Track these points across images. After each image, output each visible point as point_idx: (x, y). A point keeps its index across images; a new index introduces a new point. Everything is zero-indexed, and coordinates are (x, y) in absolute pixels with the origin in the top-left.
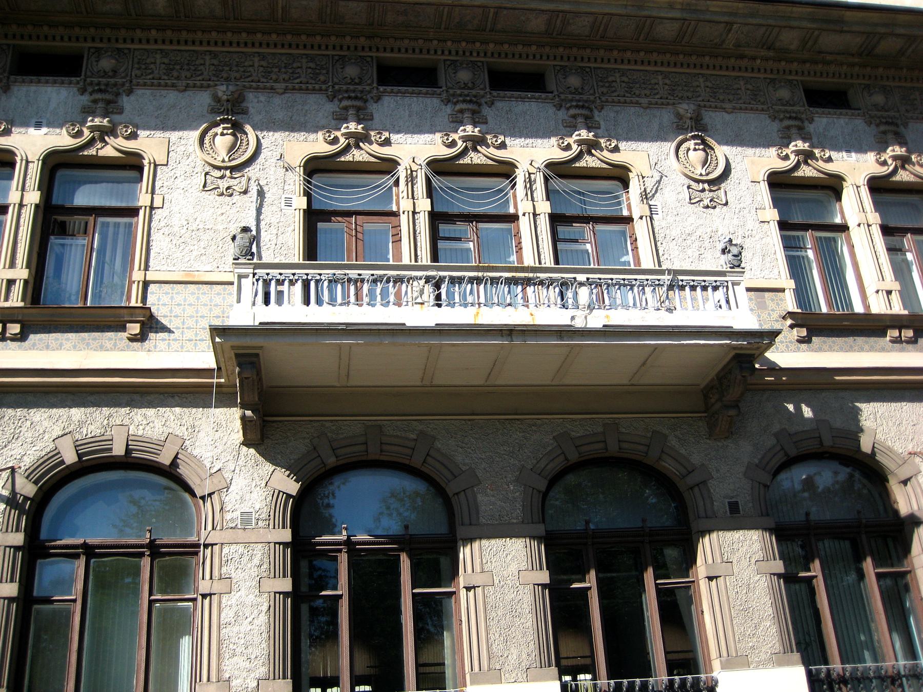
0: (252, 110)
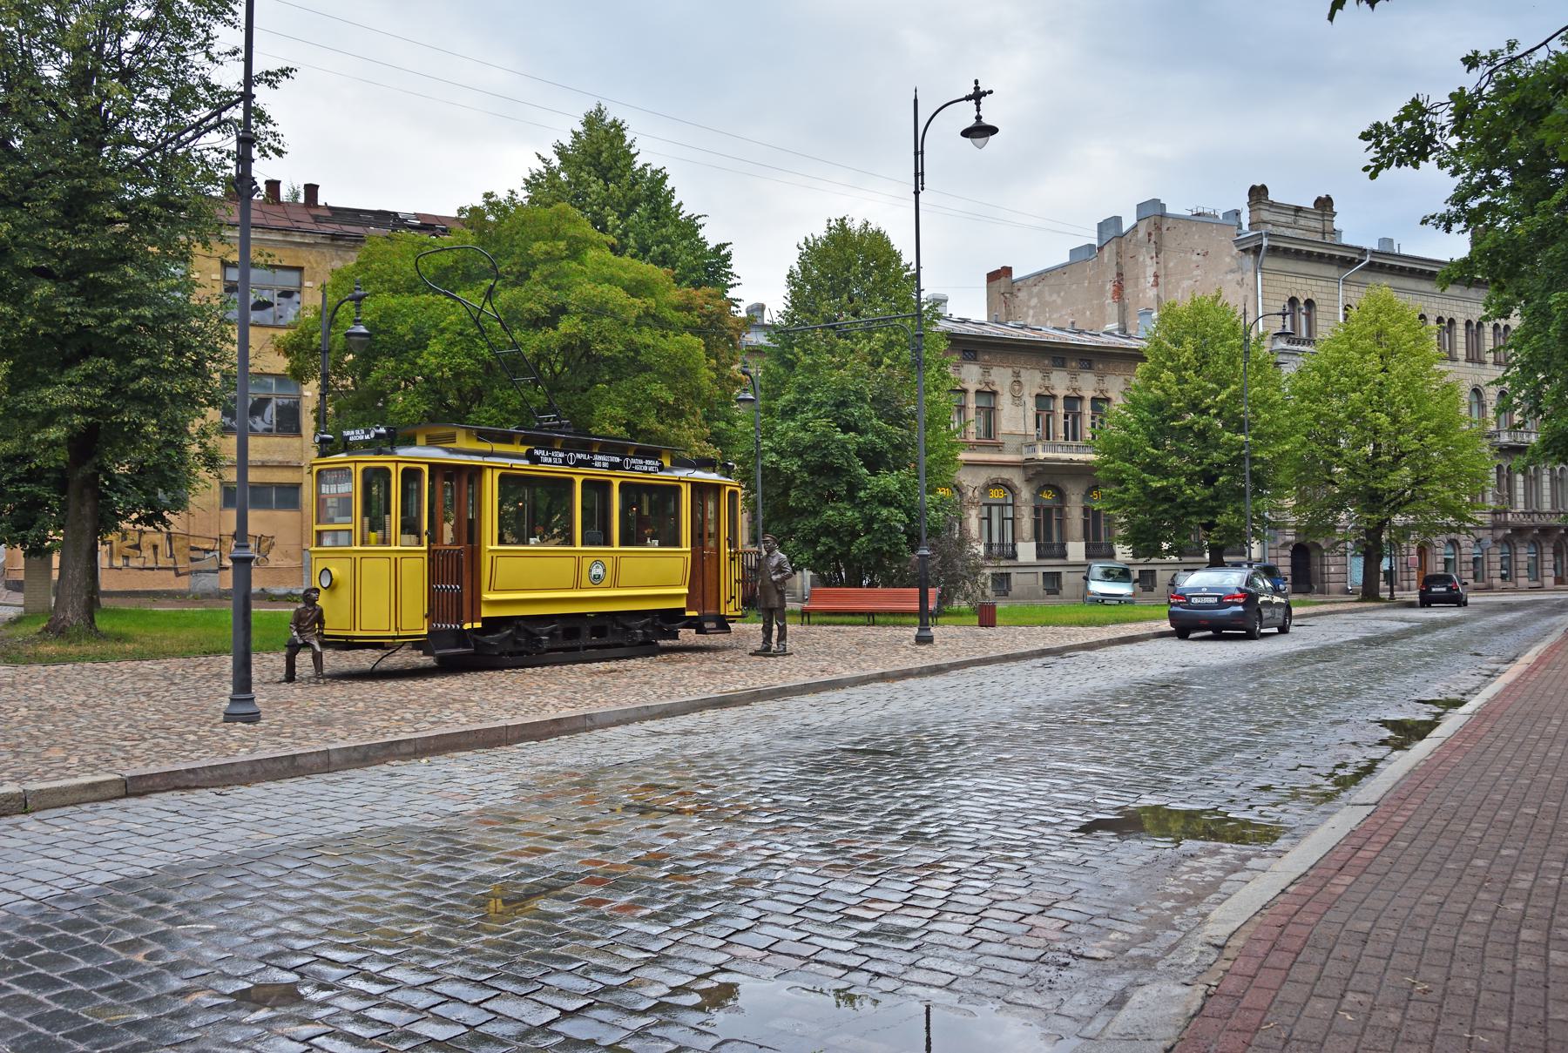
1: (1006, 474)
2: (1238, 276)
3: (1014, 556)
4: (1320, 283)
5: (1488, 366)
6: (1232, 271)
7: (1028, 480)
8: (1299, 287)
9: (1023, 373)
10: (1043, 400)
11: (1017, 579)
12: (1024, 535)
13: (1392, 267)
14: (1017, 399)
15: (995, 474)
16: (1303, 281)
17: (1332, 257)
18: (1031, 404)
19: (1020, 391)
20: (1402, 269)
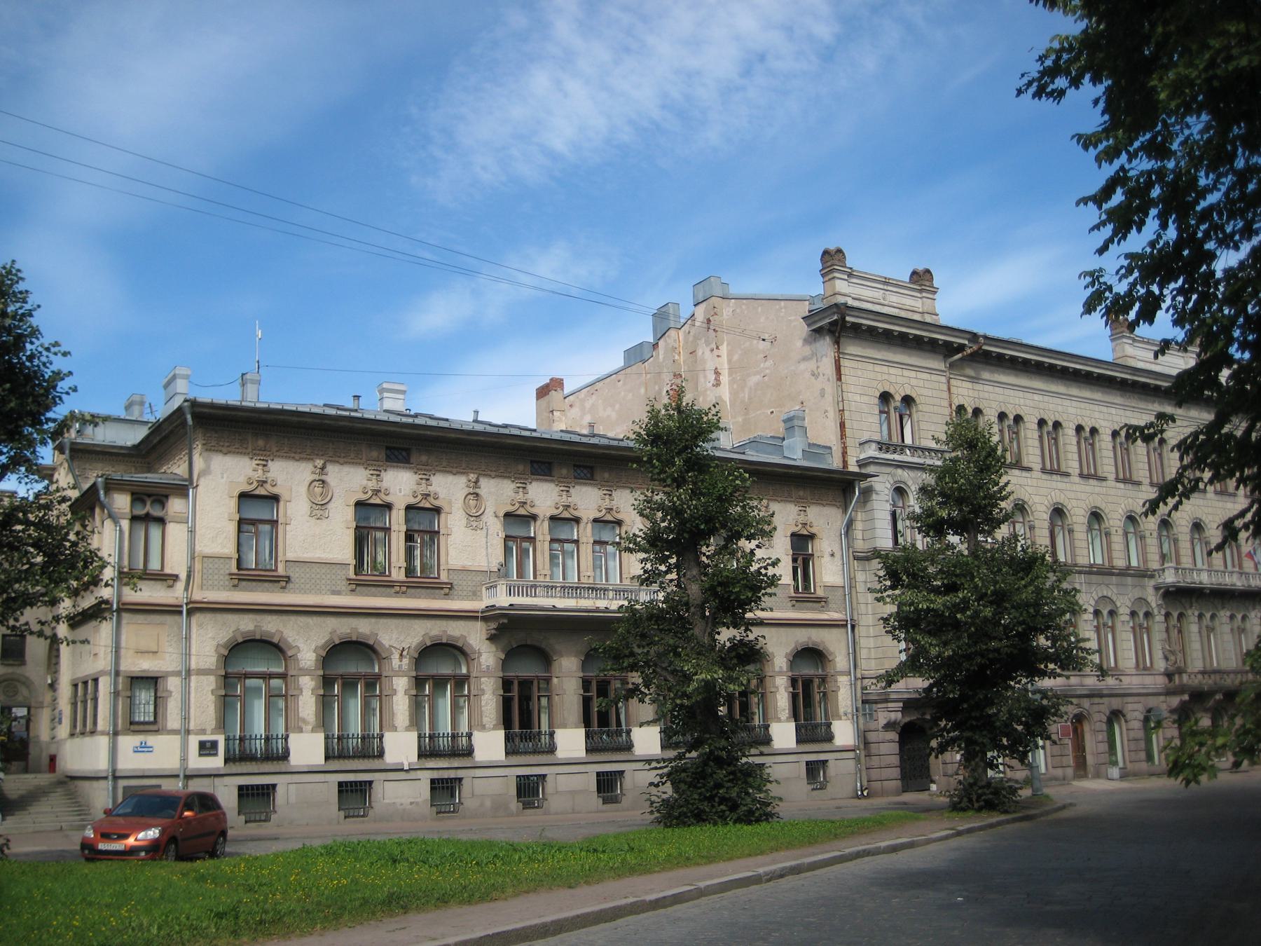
0: (482, 487)
1: (454, 630)
2: (811, 365)
3: (469, 752)
4: (921, 375)
5: (1143, 488)
6: (805, 359)
7: (492, 639)
8: (893, 379)
9: (484, 482)
10: (517, 519)
11: (287, 791)
12: (485, 720)
13: (1013, 360)
14: (475, 517)
15: (246, 625)
16: (899, 372)
17: (933, 342)
18: (496, 529)
19: (477, 507)
20: (1026, 362)
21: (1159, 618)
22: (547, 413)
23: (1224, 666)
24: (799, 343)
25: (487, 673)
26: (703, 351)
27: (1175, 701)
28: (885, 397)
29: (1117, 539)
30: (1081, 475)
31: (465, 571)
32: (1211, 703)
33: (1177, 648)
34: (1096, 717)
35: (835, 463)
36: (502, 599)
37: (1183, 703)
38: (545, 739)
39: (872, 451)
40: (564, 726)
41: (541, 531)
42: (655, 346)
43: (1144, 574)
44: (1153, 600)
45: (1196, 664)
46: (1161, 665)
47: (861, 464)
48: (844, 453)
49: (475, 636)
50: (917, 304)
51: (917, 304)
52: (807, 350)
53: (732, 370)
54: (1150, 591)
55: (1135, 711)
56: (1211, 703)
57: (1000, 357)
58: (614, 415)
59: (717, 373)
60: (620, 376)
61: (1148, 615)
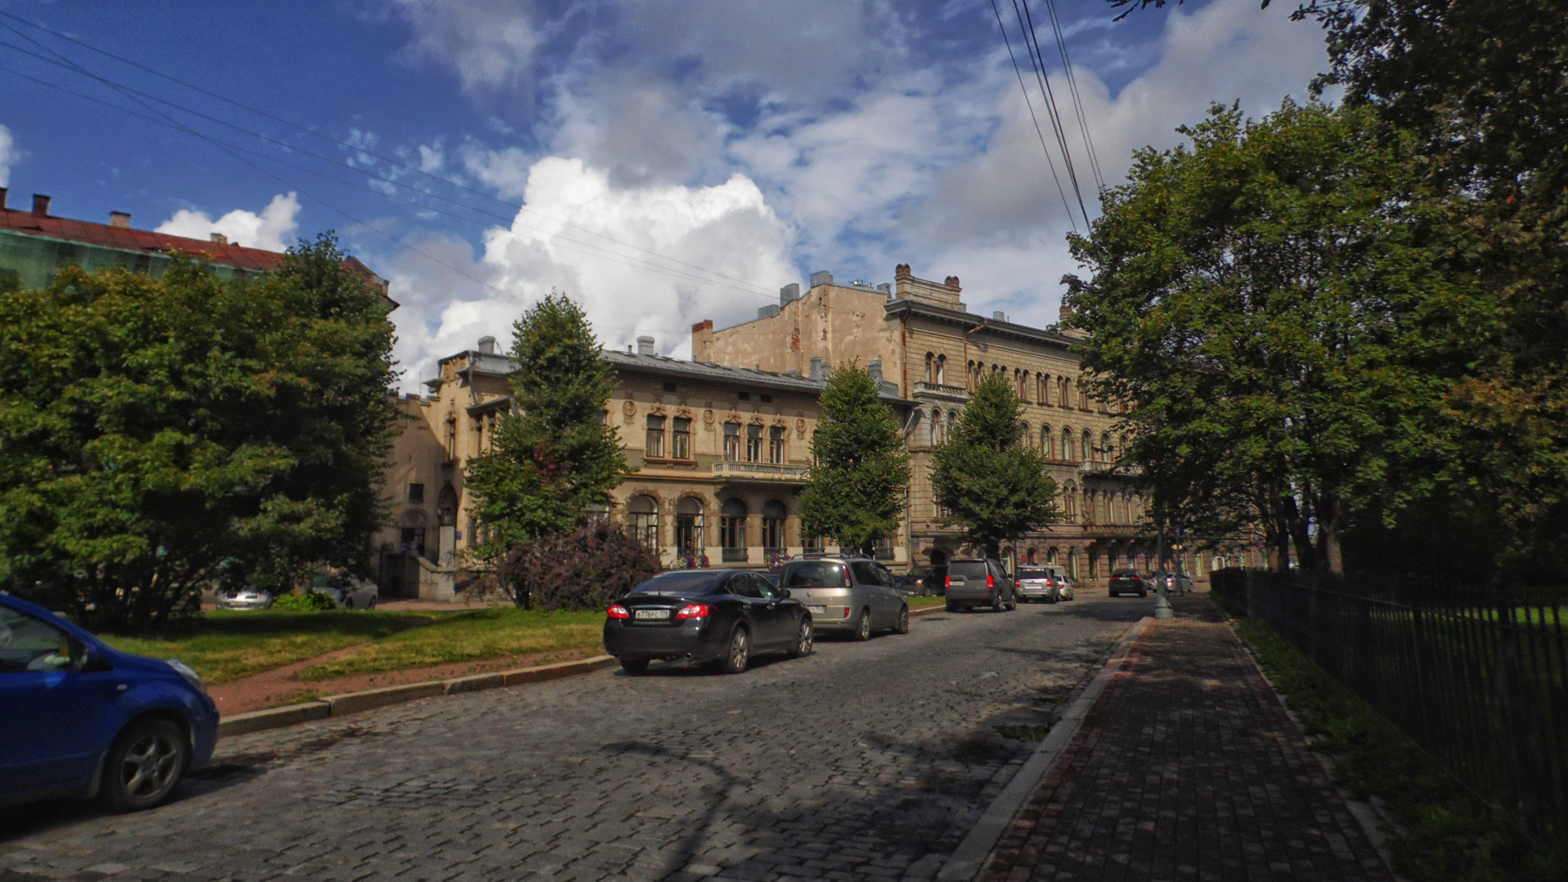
1: (697, 489)
2: (887, 334)
7: (717, 495)
13: (1003, 333)
20: (1010, 335)
21: (1081, 492)
22: (700, 346)
23: (1117, 523)
24: (880, 321)
25: (714, 514)
26: (816, 317)
27: (1087, 543)
28: (929, 355)
29: (1058, 443)
30: (1039, 404)
31: (704, 455)
32: (1109, 545)
33: (1090, 510)
34: (1042, 550)
35: (900, 395)
36: (726, 472)
37: (1093, 544)
38: (742, 553)
39: (920, 389)
40: (753, 545)
41: (668, 425)
42: (782, 309)
43: (1073, 465)
44: (1078, 481)
45: (1100, 521)
46: (1080, 520)
47: (915, 396)
48: (906, 389)
49: (709, 493)
50: (950, 298)
51: (950, 298)
52: (885, 324)
53: (833, 332)
54: (1076, 475)
55: (1064, 547)
56: (1109, 545)
57: (995, 331)
58: (749, 349)
59: (825, 332)
60: (756, 324)
61: (1074, 489)
